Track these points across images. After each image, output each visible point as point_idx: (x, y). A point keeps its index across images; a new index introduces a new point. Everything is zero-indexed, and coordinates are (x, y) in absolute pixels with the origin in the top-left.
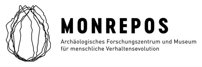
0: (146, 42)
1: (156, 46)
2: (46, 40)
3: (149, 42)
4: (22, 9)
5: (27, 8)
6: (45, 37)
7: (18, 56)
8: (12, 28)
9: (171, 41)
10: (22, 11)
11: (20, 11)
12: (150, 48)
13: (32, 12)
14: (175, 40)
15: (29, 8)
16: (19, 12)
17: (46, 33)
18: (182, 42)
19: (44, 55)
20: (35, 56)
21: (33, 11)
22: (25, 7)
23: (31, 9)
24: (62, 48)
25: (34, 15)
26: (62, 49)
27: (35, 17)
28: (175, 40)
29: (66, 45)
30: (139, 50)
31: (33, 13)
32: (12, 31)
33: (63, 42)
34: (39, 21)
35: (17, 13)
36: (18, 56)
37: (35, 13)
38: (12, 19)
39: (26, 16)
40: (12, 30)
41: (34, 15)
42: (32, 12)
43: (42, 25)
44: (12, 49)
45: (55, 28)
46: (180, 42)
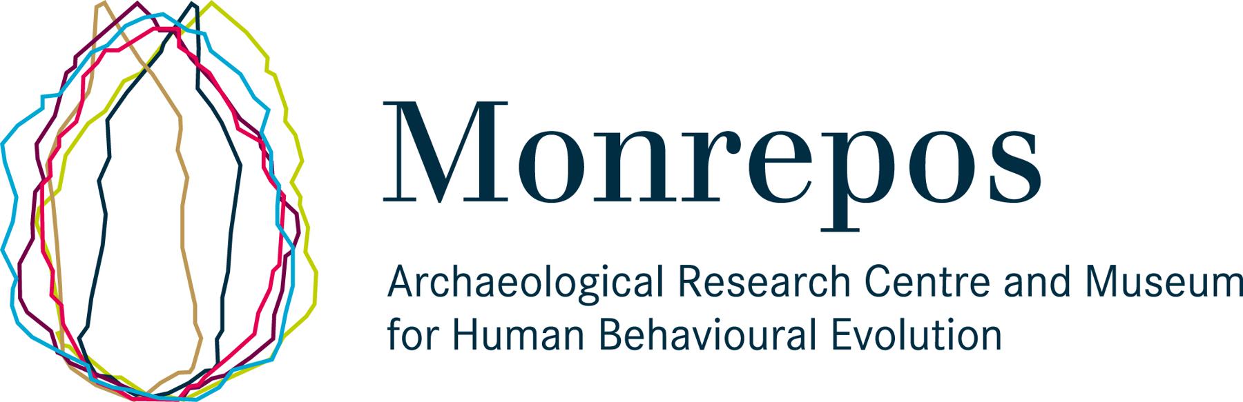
0: (927, 282)
1: (966, 310)
2: (286, 248)
3: (951, 283)
4: (114, 30)
5: (149, 24)
6: (281, 223)
7: (81, 362)
8: (44, 162)
9: (1067, 278)
10: (114, 46)
11: (100, 43)
12: (937, 328)
13: (182, 46)
14: (1091, 268)
15: (163, 22)
16: (93, 52)
17: (282, 197)
18: (1144, 285)
19: (272, 359)
20: (207, 361)
21: (189, 40)
22: (137, 12)
23: (175, 31)
24: (392, 329)
25: (201, 69)
26: (398, 335)
27: (205, 83)
28: (1091, 268)
29: (419, 310)
30: (863, 347)
31: (195, 59)
32: (40, 187)
33: (400, 281)
34: (237, 117)
35: (80, 60)
36: (81, 362)
37: (207, 60)
38: (43, 97)
39: (144, 72)
40: (45, 180)
41: (201, 69)
42: (182, 46)
43: (256, 144)
44: (49, 315)
45: (343, 159)
46: (1131, 288)
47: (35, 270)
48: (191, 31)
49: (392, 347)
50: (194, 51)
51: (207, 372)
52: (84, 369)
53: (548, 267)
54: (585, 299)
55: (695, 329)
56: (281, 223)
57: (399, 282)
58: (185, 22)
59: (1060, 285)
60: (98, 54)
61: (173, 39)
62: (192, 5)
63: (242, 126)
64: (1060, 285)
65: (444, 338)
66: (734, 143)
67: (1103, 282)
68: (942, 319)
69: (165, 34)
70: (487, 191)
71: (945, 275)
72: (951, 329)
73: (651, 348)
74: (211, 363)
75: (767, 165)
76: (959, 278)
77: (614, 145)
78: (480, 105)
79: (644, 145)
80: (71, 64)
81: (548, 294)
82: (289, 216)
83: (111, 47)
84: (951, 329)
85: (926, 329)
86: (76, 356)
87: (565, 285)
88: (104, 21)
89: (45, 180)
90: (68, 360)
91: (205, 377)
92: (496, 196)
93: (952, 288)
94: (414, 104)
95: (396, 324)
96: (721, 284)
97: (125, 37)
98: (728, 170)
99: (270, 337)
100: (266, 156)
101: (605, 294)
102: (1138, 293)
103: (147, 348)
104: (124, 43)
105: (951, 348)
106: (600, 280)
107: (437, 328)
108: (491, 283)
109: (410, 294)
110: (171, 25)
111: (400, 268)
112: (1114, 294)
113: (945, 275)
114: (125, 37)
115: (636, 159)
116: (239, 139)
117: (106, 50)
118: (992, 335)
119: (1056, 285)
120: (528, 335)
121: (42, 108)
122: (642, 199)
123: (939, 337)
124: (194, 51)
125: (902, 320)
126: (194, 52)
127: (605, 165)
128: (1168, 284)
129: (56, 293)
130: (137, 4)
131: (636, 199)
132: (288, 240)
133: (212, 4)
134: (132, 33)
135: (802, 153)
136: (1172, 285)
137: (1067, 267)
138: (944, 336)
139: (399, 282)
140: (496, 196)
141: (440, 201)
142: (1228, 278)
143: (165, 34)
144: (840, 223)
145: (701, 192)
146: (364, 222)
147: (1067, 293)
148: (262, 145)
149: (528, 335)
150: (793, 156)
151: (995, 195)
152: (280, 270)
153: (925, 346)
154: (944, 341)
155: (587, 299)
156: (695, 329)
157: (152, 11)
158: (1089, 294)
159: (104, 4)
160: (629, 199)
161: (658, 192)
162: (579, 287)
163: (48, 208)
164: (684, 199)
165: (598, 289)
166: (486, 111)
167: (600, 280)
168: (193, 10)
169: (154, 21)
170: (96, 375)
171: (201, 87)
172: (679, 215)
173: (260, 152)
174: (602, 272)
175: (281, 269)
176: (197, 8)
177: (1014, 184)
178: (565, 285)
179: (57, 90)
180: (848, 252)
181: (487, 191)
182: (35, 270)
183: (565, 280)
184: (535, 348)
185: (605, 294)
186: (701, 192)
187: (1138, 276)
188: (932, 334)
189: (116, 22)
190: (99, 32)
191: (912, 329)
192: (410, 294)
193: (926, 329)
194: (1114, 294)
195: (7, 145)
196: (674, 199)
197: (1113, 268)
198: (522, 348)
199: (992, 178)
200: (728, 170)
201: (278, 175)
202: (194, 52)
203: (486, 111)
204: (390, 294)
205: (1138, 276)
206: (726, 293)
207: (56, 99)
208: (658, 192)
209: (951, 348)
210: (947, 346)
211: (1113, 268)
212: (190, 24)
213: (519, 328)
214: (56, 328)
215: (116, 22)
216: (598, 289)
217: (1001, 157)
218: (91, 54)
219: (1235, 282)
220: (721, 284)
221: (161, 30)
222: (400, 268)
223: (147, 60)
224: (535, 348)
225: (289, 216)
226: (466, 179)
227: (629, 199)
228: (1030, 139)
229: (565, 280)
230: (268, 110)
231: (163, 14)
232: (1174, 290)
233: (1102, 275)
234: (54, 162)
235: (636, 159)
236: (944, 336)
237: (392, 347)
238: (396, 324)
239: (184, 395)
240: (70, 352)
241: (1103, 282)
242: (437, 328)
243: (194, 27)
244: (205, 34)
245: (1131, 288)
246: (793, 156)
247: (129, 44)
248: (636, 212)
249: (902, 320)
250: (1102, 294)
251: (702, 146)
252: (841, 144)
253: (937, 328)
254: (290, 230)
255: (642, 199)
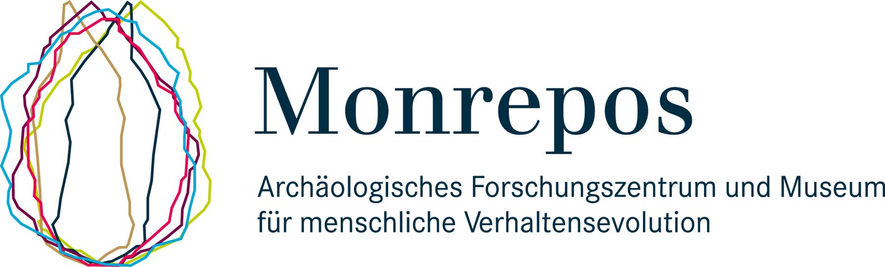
0: (650, 187)
1: (693, 207)
3: (666, 188)
4: (76, 20)
5: (99, 16)
6: (187, 149)
7: (54, 241)
9: (768, 185)
10: (76, 30)
11: (66, 29)
12: (667, 218)
13: (121, 30)
14: (784, 178)
15: (109, 15)
17: (187, 131)
19: (181, 238)
20: (138, 240)
21: (126, 26)
22: (91, 8)
23: (116, 21)
25: (133, 46)
26: (265, 223)
27: (136, 53)
28: (784, 178)
31: (130, 39)
32: (27, 124)
33: (266, 187)
34: (157, 77)
35: (53, 40)
36: (54, 241)
37: (138, 40)
38: (29, 65)
39: (96, 48)
40: (30, 119)
41: (133, 46)
42: (121, 30)
43: (170, 96)
45: (229, 106)
46: (811, 192)
47: (24, 180)
48: (127, 21)
49: (261, 231)
50: (129, 34)
51: (138, 247)
52: (56, 245)
53: (349, 177)
54: (374, 199)
55: (613, 219)
56: (187, 149)
57: (265, 187)
58: (123, 15)
59: (763, 189)
60: (65, 36)
61: (115, 26)
62: (128, 3)
63: (161, 83)
64: (763, 189)
65: (294, 225)
66: (488, 95)
67: (793, 187)
68: (674, 212)
69: (110, 23)
70: (324, 127)
71: (662, 183)
72: (676, 219)
73: (570, 231)
74: (140, 241)
75: (510, 110)
76: (671, 185)
77: (408, 96)
78: (319, 70)
79: (429, 95)
80: (47, 43)
81: (349, 195)
82: (192, 143)
83: (74, 31)
84: (676, 219)
85: (660, 219)
86: (50, 236)
87: (360, 189)
88: (70, 14)
89: (30, 119)
90: (45, 239)
91: (136, 251)
92: (330, 130)
93: (666, 191)
94: (275, 69)
95: (264, 215)
96: (446, 188)
97: (83, 25)
98: (484, 113)
99: (179, 224)
100: (177, 103)
101: (387, 195)
102: (815, 194)
103: (100, 229)
104: (82, 28)
105: (676, 231)
106: (383, 186)
107: (290, 218)
108: (326, 188)
109: (273, 196)
110: (114, 16)
111: (266, 178)
112: (799, 196)
113: (662, 183)
114: (83, 25)
115: (423, 106)
116: (157, 91)
117: (70, 33)
118: (704, 223)
119: (762, 190)
120: (316, 222)
121: (28, 72)
122: (427, 133)
123: (667, 224)
124: (129, 34)
125: (644, 213)
126: (130, 35)
127: (403, 110)
128: (835, 189)
129: (38, 195)
130: (91, 3)
131: (423, 132)
132: (192, 159)
133: (141, 2)
134: (87, 22)
135: (534, 102)
136: (837, 189)
137: (768, 177)
138: (672, 223)
139: (265, 187)
140: (330, 130)
141: (292, 133)
142: (875, 185)
143: (110, 23)
144: (559, 148)
145: (466, 127)
146: (243, 149)
147: (768, 194)
148: (174, 97)
149: (316, 222)
150: (527, 103)
151: (662, 129)
152: (186, 180)
153: (659, 230)
154: (672, 226)
155: (375, 199)
156: (613, 219)
157: (101, 8)
158: (783, 196)
159: (69, 2)
160: (419, 133)
161: (438, 127)
162: (369, 191)
163: (32, 138)
164: (455, 133)
165: (382, 192)
166: (323, 74)
167: (383, 186)
168: (128, 6)
169: (103, 14)
170: (64, 249)
171: (134, 58)
172: (452, 142)
173: (173, 101)
174: (385, 181)
175: (187, 179)
176: (131, 5)
177: (674, 122)
178: (360, 189)
179: (38, 60)
180: (559, 170)
181: (324, 127)
182: (24, 180)
183: (360, 186)
184: (516, 231)
185: (387, 195)
186: (466, 127)
187: (815, 183)
188: (664, 222)
189: (77, 15)
190: (66, 21)
191: (651, 219)
192: (273, 196)
193: (660, 219)
194: (799, 196)
195: (4, 97)
196: (448, 133)
197: (798, 178)
198: (311, 231)
199: (660, 118)
200: (484, 113)
201: (185, 116)
202: (130, 35)
203: (323, 74)
204: (259, 196)
205: (815, 183)
206: (449, 195)
207: (37, 66)
208: (438, 127)
209: (676, 231)
210: (674, 230)
211: (798, 178)
212: (127, 16)
213: (309, 218)
214: (37, 218)
215: (77, 15)
216: (382, 192)
217: (665, 104)
218: (61, 36)
219: (880, 188)
220: (446, 188)
221: (107, 20)
222: (266, 178)
223: (97, 40)
224: (516, 231)
225: (192, 143)
226: (310, 119)
227: (419, 133)
228: (685, 92)
229: (360, 186)
230: (178, 73)
231: (108, 10)
232: (840, 192)
233: (791, 182)
234: (36, 107)
235: (423, 106)
236: (672, 223)
237: (261, 231)
238: (264, 215)
239: (122, 262)
240: (46, 234)
241: (793, 187)
242: (290, 218)
243: (129, 18)
244: (136, 23)
245: (811, 192)
246: (527, 103)
247: (86, 29)
248: (423, 140)
249: (644, 213)
250: (791, 195)
251: (467, 97)
252: (559, 95)
253: (667, 218)
254: (193, 153)
255: (427, 133)
